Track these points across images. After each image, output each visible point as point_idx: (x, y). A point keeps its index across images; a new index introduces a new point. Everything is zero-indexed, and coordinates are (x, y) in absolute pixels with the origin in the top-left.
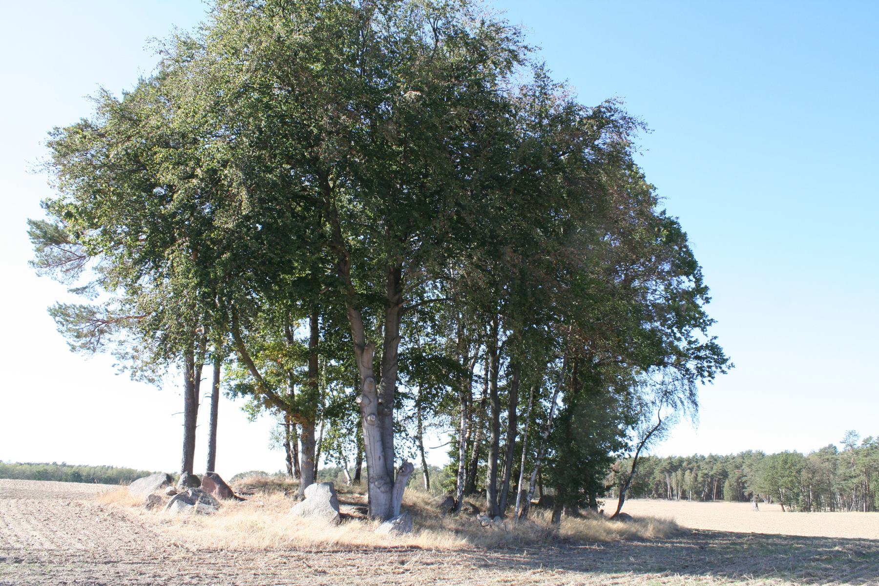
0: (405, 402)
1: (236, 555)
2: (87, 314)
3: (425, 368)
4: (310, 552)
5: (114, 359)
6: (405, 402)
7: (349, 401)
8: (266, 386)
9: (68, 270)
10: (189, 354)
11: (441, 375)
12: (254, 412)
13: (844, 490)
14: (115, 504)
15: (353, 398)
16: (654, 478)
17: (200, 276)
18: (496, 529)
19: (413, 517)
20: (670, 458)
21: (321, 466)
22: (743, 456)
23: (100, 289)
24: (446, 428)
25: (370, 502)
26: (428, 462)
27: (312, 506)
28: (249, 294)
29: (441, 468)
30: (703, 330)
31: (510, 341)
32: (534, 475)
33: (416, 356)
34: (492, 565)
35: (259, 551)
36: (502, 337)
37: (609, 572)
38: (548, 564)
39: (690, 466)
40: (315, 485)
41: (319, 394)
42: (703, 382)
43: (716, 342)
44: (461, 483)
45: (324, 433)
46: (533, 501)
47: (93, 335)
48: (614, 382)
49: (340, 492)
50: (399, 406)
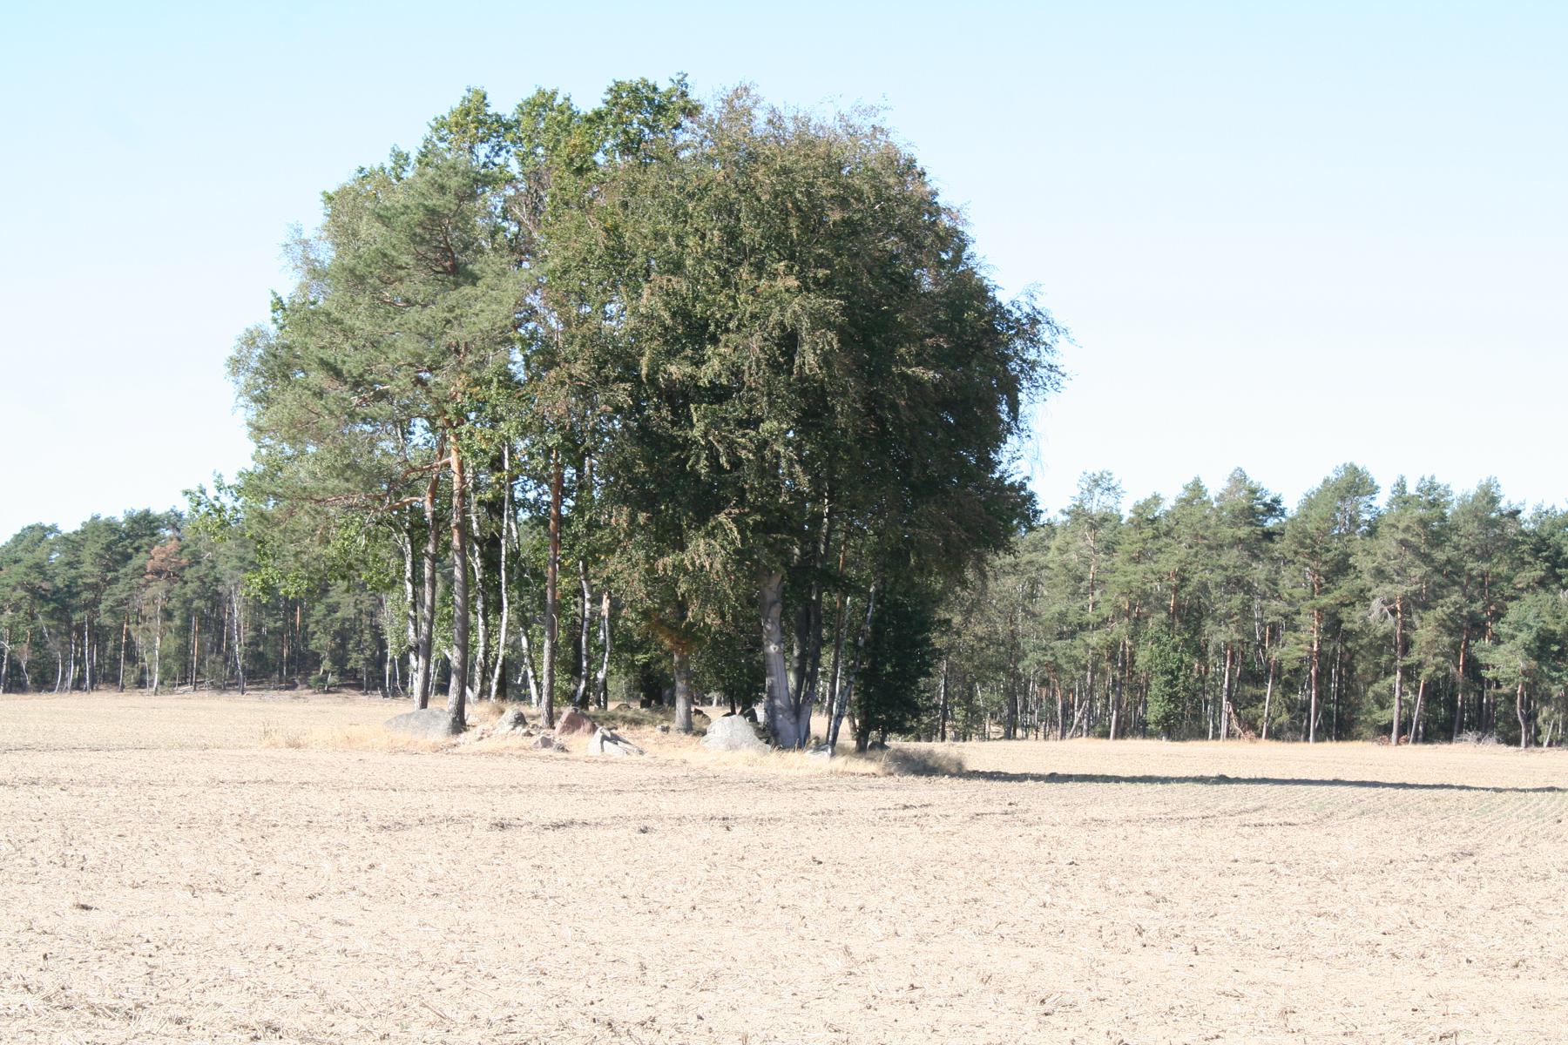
13: (1057, 669)
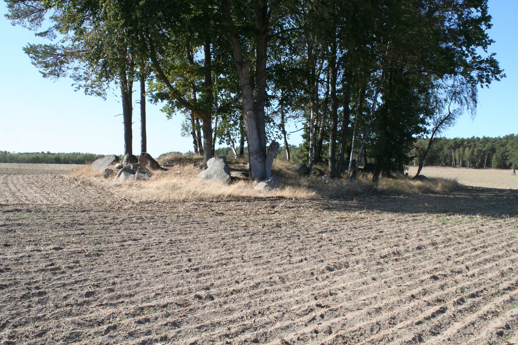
0: (272, 102)
1: (164, 204)
2: (50, 51)
3: (285, 77)
4: (213, 202)
5: (72, 81)
6: (272, 102)
7: (234, 102)
8: (176, 93)
9: (33, 20)
10: (123, 75)
11: (296, 84)
12: (170, 112)
14: (85, 176)
15: (236, 99)
16: (444, 153)
17: (125, 18)
18: (335, 186)
19: (278, 179)
20: (455, 139)
21: (217, 146)
22: (507, 138)
23: (56, 32)
24: (300, 118)
25: (250, 168)
26: (289, 143)
27: (212, 172)
28: (160, 30)
29: (298, 146)
30: (485, 47)
31: (344, 58)
32: (360, 150)
33: (279, 69)
34: (332, 208)
35: (179, 202)
36: (339, 54)
37: (411, 212)
38: (370, 208)
39: (469, 144)
40: (214, 158)
41: (213, 98)
42: (482, 87)
43: (494, 57)
44: (311, 155)
45: (218, 124)
46: (360, 167)
47: (56, 65)
48: (418, 86)
49: (230, 163)
50: (269, 105)
